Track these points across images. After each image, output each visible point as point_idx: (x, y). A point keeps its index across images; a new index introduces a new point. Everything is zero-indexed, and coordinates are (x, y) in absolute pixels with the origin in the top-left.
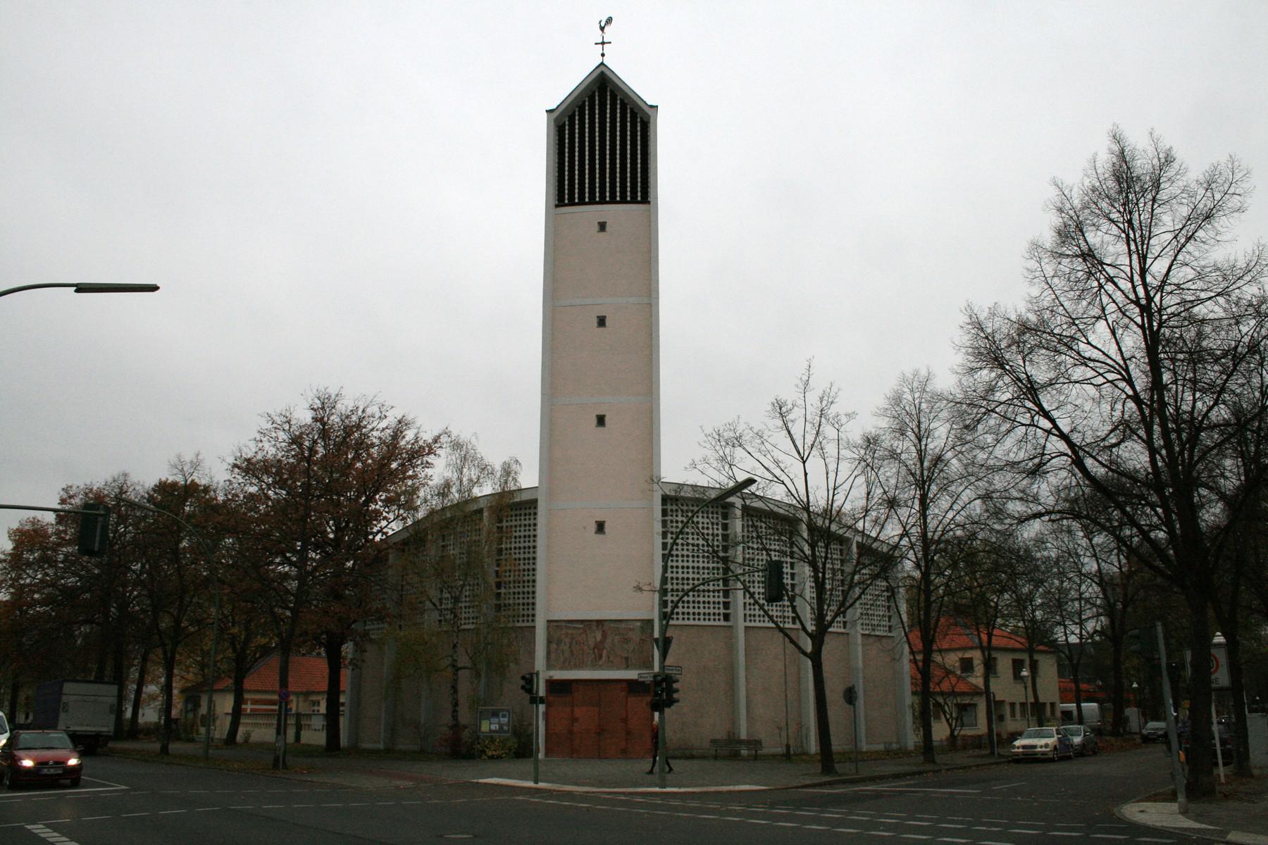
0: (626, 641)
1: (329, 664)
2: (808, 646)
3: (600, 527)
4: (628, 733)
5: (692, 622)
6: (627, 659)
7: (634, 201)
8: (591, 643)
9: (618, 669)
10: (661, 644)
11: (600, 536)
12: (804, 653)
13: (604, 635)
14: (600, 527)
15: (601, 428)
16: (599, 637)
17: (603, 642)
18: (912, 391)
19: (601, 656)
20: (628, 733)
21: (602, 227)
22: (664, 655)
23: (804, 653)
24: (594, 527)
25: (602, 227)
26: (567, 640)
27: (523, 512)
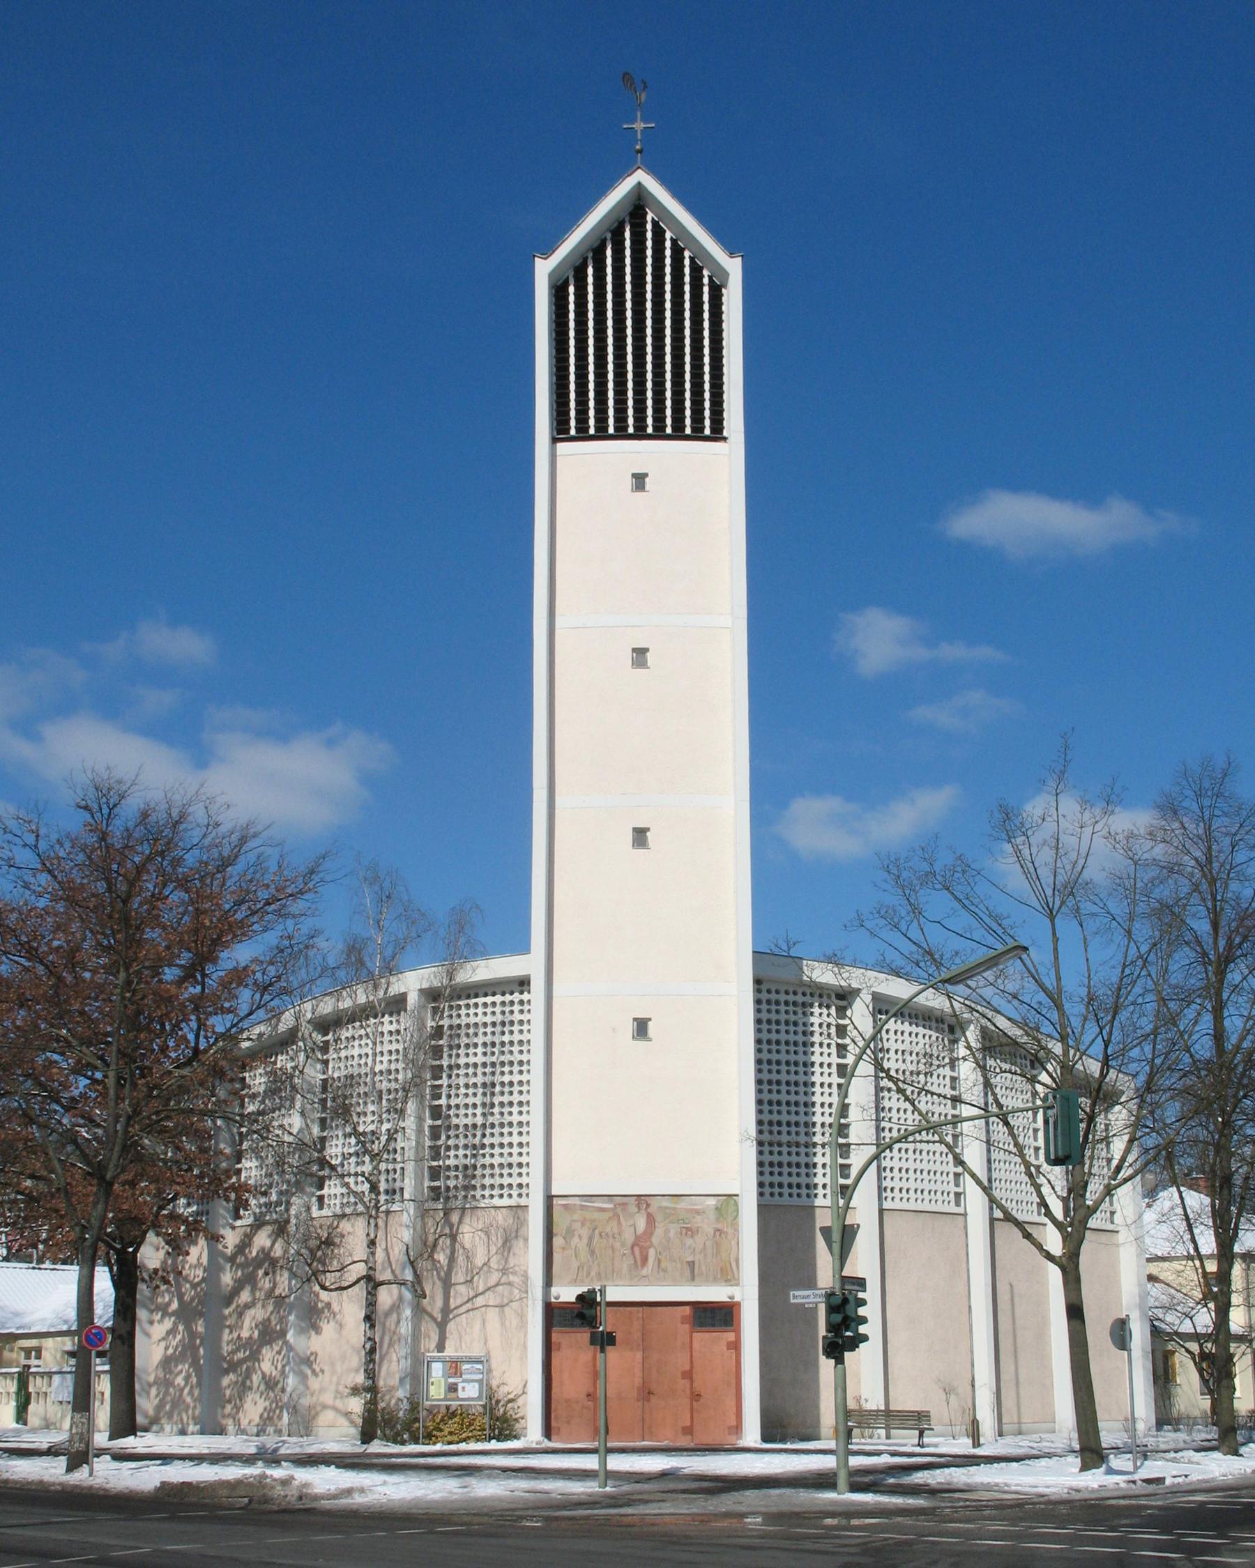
0: (690, 1231)
1: (1217, 1235)
2: (1054, 1242)
3: (641, 1028)
4: (696, 1397)
5: (786, 1200)
6: (692, 1264)
7: (697, 435)
8: (629, 1237)
9: (675, 1282)
10: (836, 1236)
11: (641, 1044)
12: (1049, 1257)
13: (651, 1220)
14: (641, 1028)
15: (641, 852)
16: (641, 1223)
17: (649, 1232)
18: (1199, 795)
19: (645, 1260)
20: (696, 1397)
21: (639, 481)
22: (843, 1256)
23: (1049, 1257)
24: (630, 1027)
25: (639, 481)
26: (585, 1233)
27: (481, 1000)
